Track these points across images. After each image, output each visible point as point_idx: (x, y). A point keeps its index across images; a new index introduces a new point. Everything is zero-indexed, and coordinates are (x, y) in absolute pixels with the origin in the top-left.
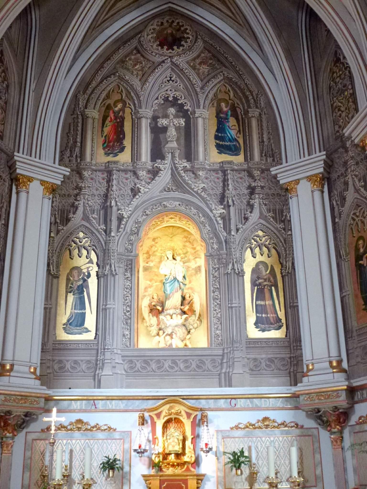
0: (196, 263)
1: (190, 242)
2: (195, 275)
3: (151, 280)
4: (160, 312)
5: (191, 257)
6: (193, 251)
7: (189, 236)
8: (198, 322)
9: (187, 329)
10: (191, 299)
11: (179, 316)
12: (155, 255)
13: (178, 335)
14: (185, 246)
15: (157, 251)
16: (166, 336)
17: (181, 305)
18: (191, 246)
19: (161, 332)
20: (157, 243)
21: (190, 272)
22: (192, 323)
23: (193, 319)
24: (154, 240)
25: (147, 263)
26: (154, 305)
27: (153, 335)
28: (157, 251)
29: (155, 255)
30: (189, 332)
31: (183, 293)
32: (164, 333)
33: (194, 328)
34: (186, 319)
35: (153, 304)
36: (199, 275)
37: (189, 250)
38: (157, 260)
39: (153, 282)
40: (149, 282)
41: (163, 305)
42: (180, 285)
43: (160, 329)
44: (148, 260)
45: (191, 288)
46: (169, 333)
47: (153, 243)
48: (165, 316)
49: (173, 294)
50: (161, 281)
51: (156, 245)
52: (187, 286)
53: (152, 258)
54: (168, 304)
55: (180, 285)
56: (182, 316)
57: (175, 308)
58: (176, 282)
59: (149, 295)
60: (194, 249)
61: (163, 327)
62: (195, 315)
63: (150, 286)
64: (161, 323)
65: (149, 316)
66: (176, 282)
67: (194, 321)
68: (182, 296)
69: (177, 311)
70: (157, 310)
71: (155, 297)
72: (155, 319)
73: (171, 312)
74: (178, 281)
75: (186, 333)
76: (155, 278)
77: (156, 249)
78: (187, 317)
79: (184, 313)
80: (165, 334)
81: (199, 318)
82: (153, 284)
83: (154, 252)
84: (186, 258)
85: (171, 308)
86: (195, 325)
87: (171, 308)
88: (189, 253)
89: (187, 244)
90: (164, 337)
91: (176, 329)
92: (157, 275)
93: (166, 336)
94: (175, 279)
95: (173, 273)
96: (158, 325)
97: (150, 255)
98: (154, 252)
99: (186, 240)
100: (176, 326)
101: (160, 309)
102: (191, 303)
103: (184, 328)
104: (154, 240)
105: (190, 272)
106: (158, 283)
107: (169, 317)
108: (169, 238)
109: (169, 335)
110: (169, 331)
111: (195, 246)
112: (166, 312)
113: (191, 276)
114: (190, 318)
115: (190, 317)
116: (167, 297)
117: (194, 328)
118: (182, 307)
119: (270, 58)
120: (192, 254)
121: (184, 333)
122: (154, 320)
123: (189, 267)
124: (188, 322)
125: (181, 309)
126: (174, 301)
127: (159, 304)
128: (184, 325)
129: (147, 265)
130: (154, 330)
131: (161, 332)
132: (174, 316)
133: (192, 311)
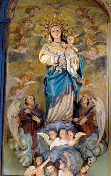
0: (98, 52)
1: (88, 17)
2: (96, 71)
3: (21, 77)
4: (40, 126)
5: (89, 42)
6: (93, 33)
7: (87, 8)
8: (102, 146)
9: (82, 156)
10: (90, 106)
11: (71, 133)
12: (30, 36)
13: (69, 164)
14: (79, 23)
15: (33, 29)
16: (47, 165)
17: (74, 116)
18: (91, 24)
19: (39, 160)
20: (32, 16)
21: (87, 67)
22: (92, 147)
23: (93, 140)
24: (28, 10)
25: (16, 48)
26: (28, 114)
27: (24, 165)
28: (33, 29)
29: (30, 36)
30: (86, 162)
31: (76, 97)
32: (44, 161)
33: (94, 155)
34: (81, 140)
35: (27, 111)
36: (102, 73)
37: (86, 30)
38: (33, 44)
39: (25, 79)
40: (18, 80)
41: (43, 115)
42: (72, 82)
43: (36, 155)
44: (18, 44)
45: (89, 93)
46: (54, 161)
47: (27, 15)
48: (46, 132)
49: (62, 97)
50: (39, 79)
51: (31, 19)
52: (82, 89)
53: (24, 40)
54: (53, 112)
55: (72, 82)
56: (75, 133)
57: (64, 120)
58: (67, 77)
59: (19, 100)
60: (95, 29)
61: (42, 151)
62: (97, 133)
63: (21, 87)
64: (39, 146)
65: (19, 132)
66: (67, 77)
67: (95, 143)
68: (75, 103)
69: (67, 124)
70: (33, 122)
71: (30, 102)
72: (29, 137)
73: (58, 125)
74: (70, 76)
75: (82, 162)
76: (29, 73)
77: (32, 25)
78: (82, 137)
79: (78, 128)
80: (46, 163)
81: (103, 139)
82: (25, 82)
83: (28, 30)
84: (81, 44)
85: (57, 120)
86: (97, 151)
87: (57, 120)
88: (86, 36)
89: (84, 20)
90: (44, 168)
91: (66, 154)
92: (32, 69)
93: (47, 165)
94: (65, 72)
95: (62, 62)
96: (33, 148)
97: (21, 36)
98: (28, 30)
99: (81, 13)
100: (65, 149)
101: (38, 121)
102: (91, 113)
103: (78, 154)
104: (28, 10)
105: (87, 67)
106: (33, 82)
107: (53, 133)
108: (53, 10)
109: (54, 164)
110: (54, 157)
111: (96, 24)
112: (47, 127)
113: (89, 72)
114: (88, 139)
115: (88, 136)
116: (50, 102)
117: (94, 155)
118: (76, 120)
119: (104, 125)
120: (92, 37)
121: (78, 163)
122: (26, 140)
123: (85, 58)
124: (84, 144)
125: (73, 122)
126: (64, 106)
127: (37, 113)
128: (78, 150)
129: (16, 51)
130: (26, 156)
131: (39, 160)
132: (62, 132)
133: (92, 127)
